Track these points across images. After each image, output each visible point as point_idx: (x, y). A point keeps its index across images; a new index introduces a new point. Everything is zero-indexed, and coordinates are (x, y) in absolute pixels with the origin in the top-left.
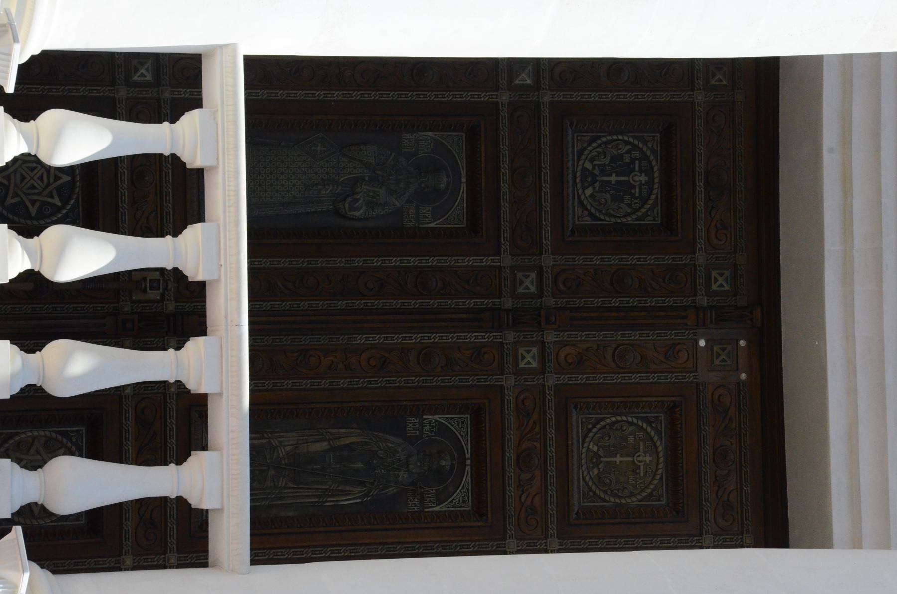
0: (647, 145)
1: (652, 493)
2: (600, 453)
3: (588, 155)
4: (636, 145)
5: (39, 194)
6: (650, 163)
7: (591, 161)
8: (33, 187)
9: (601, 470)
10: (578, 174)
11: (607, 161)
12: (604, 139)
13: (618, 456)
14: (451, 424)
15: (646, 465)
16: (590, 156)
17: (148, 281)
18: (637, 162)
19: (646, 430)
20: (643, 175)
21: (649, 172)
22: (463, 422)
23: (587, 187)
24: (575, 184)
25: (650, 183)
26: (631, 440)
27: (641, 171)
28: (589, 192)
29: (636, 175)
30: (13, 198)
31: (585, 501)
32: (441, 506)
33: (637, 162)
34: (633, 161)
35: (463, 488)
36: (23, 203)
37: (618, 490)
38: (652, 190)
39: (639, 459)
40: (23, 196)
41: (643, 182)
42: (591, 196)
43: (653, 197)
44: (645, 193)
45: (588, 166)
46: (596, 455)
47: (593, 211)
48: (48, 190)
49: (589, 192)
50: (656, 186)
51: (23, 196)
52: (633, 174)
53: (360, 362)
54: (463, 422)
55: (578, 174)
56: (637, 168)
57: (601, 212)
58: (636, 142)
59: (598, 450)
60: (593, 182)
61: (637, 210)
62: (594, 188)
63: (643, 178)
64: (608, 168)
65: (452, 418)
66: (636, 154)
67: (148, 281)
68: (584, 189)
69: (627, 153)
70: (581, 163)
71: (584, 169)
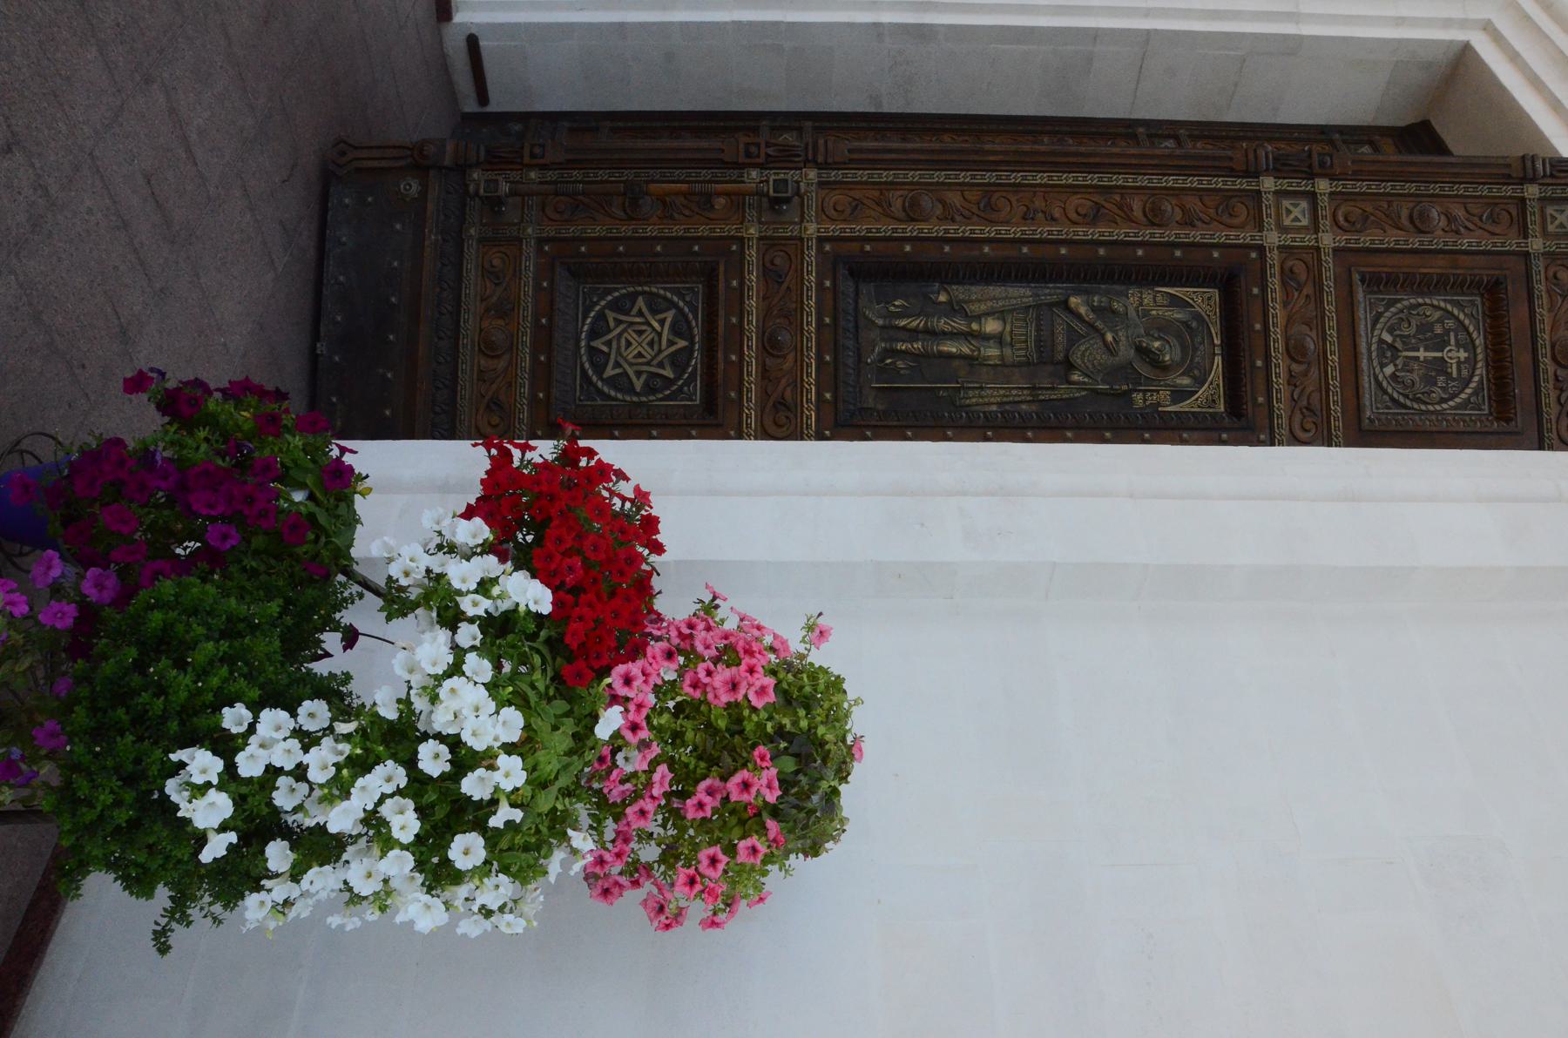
0: (1463, 311)
1: (1469, 399)
2: (1396, 345)
3: (1386, 323)
4: (1448, 312)
5: (648, 364)
6: (1469, 334)
7: (1391, 331)
8: (640, 333)
9: (1400, 367)
10: (1374, 347)
11: (1413, 330)
12: (1406, 303)
13: (1422, 349)
14: (1193, 299)
15: (1459, 363)
16: (1389, 324)
17: (771, 183)
18: (1452, 334)
19: (1457, 318)
20: (1462, 350)
21: (1470, 346)
22: (1209, 299)
23: (1386, 365)
24: (1370, 359)
25: (1471, 361)
26: (1438, 330)
27: (1458, 345)
28: (1389, 370)
29: (1450, 351)
30: (613, 368)
31: (1379, 405)
32: (1181, 404)
33: (1452, 334)
34: (1447, 332)
35: (1211, 383)
36: (625, 374)
37: (1423, 393)
38: (1474, 369)
39: (1450, 355)
40: (626, 366)
41: (1462, 359)
42: (1394, 376)
43: (1476, 379)
44: (1465, 373)
45: (1388, 338)
46: (1392, 347)
47: (1395, 395)
48: (656, 325)
49: (1389, 370)
50: (1480, 365)
51: (626, 366)
52: (1448, 348)
53: (1064, 209)
54: (1209, 299)
55: (1374, 347)
56: (1453, 341)
57: (1406, 396)
58: (1449, 307)
59: (1394, 341)
60: (1393, 360)
61: (1452, 397)
62: (1395, 365)
63: (1463, 355)
64: (1413, 341)
65: (1194, 292)
66: (1450, 323)
67: (771, 183)
68: (1382, 366)
69: (1438, 321)
70: (1376, 333)
71: (1381, 341)
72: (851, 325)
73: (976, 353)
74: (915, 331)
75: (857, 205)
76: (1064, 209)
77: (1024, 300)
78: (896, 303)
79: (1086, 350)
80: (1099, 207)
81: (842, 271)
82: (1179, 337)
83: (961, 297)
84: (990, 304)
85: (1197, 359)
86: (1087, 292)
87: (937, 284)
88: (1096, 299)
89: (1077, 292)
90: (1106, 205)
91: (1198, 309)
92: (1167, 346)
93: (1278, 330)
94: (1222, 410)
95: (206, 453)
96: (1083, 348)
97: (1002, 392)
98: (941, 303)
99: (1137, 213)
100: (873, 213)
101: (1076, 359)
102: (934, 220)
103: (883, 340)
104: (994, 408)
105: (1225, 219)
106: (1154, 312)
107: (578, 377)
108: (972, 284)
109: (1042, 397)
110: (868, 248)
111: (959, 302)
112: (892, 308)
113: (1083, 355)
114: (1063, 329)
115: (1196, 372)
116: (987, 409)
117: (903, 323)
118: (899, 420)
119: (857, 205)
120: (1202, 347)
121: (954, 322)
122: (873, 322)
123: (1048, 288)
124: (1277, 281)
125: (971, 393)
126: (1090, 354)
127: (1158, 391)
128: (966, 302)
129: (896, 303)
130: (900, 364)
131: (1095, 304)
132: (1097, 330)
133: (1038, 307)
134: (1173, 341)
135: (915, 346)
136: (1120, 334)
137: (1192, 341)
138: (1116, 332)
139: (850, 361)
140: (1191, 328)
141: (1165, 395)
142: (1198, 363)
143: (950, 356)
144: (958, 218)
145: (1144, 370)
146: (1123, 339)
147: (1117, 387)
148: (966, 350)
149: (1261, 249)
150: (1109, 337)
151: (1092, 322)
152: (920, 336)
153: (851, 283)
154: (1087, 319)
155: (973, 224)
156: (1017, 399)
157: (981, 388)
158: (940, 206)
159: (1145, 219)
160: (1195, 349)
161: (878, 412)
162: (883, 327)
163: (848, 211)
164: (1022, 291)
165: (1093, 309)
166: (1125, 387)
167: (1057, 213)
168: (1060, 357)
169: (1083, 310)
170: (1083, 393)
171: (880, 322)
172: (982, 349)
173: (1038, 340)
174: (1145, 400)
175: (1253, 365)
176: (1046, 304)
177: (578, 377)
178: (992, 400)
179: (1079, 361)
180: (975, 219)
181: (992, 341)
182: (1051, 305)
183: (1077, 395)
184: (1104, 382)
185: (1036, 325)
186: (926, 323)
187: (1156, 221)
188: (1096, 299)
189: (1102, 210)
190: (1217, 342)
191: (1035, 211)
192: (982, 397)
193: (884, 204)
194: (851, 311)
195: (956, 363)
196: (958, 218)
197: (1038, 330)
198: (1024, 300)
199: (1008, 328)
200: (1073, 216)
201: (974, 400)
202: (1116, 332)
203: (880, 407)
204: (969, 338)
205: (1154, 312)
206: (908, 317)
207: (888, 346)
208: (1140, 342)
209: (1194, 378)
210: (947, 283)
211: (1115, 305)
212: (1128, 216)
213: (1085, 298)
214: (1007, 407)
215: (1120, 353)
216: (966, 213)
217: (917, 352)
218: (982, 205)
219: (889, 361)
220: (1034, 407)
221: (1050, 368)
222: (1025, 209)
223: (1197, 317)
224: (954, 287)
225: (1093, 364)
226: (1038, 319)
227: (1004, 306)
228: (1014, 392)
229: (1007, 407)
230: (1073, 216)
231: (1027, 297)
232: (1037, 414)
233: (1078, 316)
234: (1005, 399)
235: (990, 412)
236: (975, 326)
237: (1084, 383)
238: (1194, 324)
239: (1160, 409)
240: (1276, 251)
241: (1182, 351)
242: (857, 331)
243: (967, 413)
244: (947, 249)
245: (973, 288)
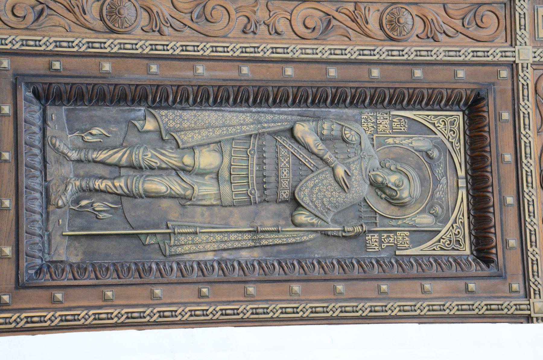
22: (452, 123)
35: (455, 222)
53: (290, 21)
54: (452, 123)
65: (436, 116)
72: (39, 159)
73: (189, 193)
74: (117, 166)
75: (42, 11)
76: (290, 21)
77: (245, 128)
78: (94, 132)
79: (315, 185)
80: (329, 19)
81: (25, 93)
82: (418, 168)
83: (171, 124)
84: (204, 133)
85: (438, 195)
86: (317, 118)
87: (143, 108)
88: (326, 126)
89: (303, 118)
90: (336, 15)
91: (440, 135)
92: (406, 181)
93: (531, 162)
94: (468, 252)
95: (455, 106)
96: (311, 184)
97: (219, 237)
98: (147, 132)
99: (373, 26)
100: (63, 22)
101: (303, 196)
102: (138, 31)
103: (77, 176)
104: (210, 256)
105: (472, 31)
106: (390, 141)
107: (429, 197)
108: (183, 109)
109: (264, 242)
110: (57, 65)
111: (168, 132)
112: (88, 138)
113: (311, 192)
114: (288, 162)
115: (438, 209)
116: (201, 257)
117: (102, 156)
118: (97, 278)
119: (42, 11)
120: (444, 180)
121: (163, 154)
122: (65, 155)
123: (272, 113)
124: (531, 104)
125: (182, 239)
126: (320, 191)
127: (395, 232)
128: (177, 131)
129: (94, 132)
130: (99, 206)
131: (325, 132)
132: (326, 163)
133: (259, 135)
134: (412, 174)
135: (117, 184)
136: (353, 167)
137: (433, 174)
138: (348, 166)
139: (37, 206)
140: (431, 158)
141: (403, 237)
142: (440, 198)
143: (159, 196)
144: (167, 30)
145: (381, 207)
146: (356, 173)
147: (351, 229)
148: (177, 188)
149: (513, 67)
150: (340, 171)
151: (321, 153)
152: (123, 171)
153: (36, 107)
154: (315, 150)
155: (185, 38)
156: (236, 245)
157: (195, 233)
158: (145, 15)
159: (381, 33)
160: (437, 182)
161: (71, 266)
162: (79, 161)
163: (31, 17)
164: (242, 116)
165: (323, 139)
166: (358, 229)
167: (282, 25)
168: (285, 195)
169: (311, 140)
170: (312, 236)
171: (74, 155)
172: (196, 187)
173: (262, 178)
174: (381, 242)
175: (503, 201)
176: (269, 133)
177: (429, 197)
178: (208, 247)
179: (307, 200)
180: (187, 31)
181: (207, 177)
182: (274, 134)
183: (305, 238)
184: (335, 221)
185: (258, 158)
186: (131, 154)
187: (394, 35)
188: (326, 126)
189: (334, 22)
190: (462, 173)
191: (257, 23)
192: (196, 244)
193: (76, 10)
194: (37, 143)
195: (165, 203)
196: (167, 30)
197: (261, 163)
198: (245, 128)
199: (226, 160)
200: (300, 29)
201: (187, 248)
202: (348, 166)
203: (74, 259)
204: (181, 174)
205: (390, 141)
206: (107, 148)
207: (84, 184)
208: (375, 176)
209: (436, 216)
210: (155, 108)
211: (348, 134)
212: (363, 30)
213: (313, 124)
214: (225, 255)
215: (353, 190)
216: (177, 25)
217: (120, 191)
218: (195, 16)
219: (84, 203)
220: (256, 254)
221: (273, 207)
222: (246, 20)
223: (440, 146)
224: (163, 112)
225: (323, 203)
226: (261, 151)
227: (221, 135)
228: (233, 237)
229: (225, 255)
230: (300, 29)
231: (247, 125)
232: (259, 263)
233: (306, 147)
234: (223, 246)
235: (205, 263)
236: (188, 160)
237: (313, 225)
238: (435, 154)
239: (398, 253)
240: (530, 69)
241: (422, 185)
242: (45, 167)
243: (178, 264)
244: (154, 68)
245: (186, 114)
